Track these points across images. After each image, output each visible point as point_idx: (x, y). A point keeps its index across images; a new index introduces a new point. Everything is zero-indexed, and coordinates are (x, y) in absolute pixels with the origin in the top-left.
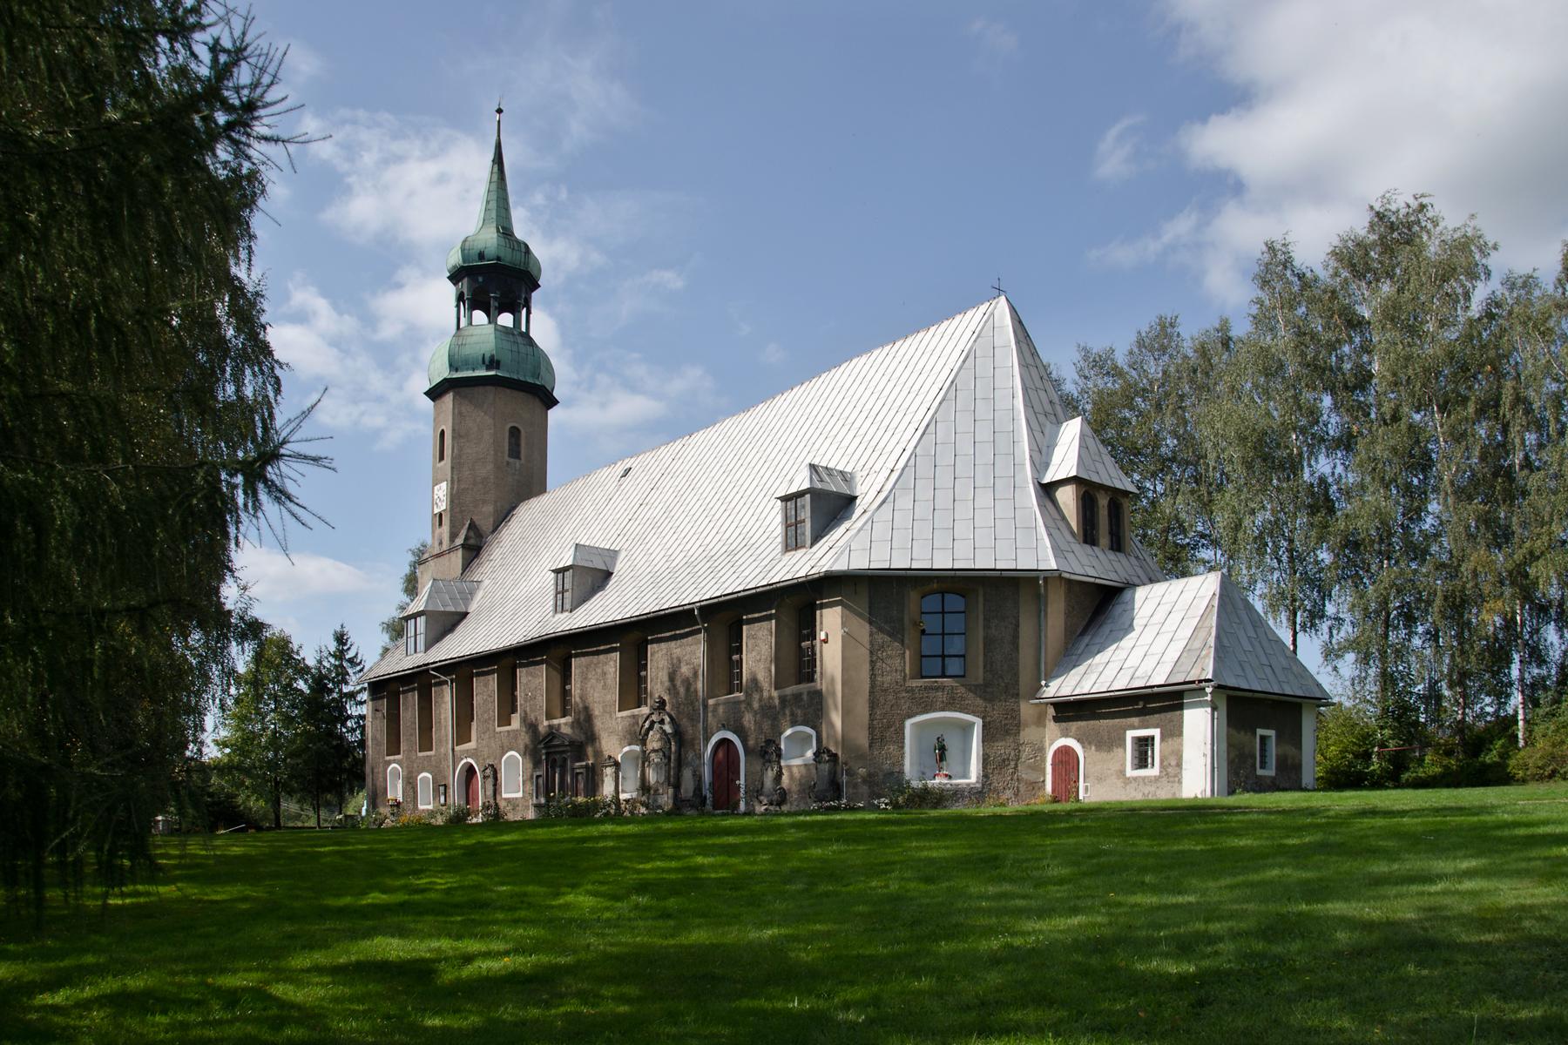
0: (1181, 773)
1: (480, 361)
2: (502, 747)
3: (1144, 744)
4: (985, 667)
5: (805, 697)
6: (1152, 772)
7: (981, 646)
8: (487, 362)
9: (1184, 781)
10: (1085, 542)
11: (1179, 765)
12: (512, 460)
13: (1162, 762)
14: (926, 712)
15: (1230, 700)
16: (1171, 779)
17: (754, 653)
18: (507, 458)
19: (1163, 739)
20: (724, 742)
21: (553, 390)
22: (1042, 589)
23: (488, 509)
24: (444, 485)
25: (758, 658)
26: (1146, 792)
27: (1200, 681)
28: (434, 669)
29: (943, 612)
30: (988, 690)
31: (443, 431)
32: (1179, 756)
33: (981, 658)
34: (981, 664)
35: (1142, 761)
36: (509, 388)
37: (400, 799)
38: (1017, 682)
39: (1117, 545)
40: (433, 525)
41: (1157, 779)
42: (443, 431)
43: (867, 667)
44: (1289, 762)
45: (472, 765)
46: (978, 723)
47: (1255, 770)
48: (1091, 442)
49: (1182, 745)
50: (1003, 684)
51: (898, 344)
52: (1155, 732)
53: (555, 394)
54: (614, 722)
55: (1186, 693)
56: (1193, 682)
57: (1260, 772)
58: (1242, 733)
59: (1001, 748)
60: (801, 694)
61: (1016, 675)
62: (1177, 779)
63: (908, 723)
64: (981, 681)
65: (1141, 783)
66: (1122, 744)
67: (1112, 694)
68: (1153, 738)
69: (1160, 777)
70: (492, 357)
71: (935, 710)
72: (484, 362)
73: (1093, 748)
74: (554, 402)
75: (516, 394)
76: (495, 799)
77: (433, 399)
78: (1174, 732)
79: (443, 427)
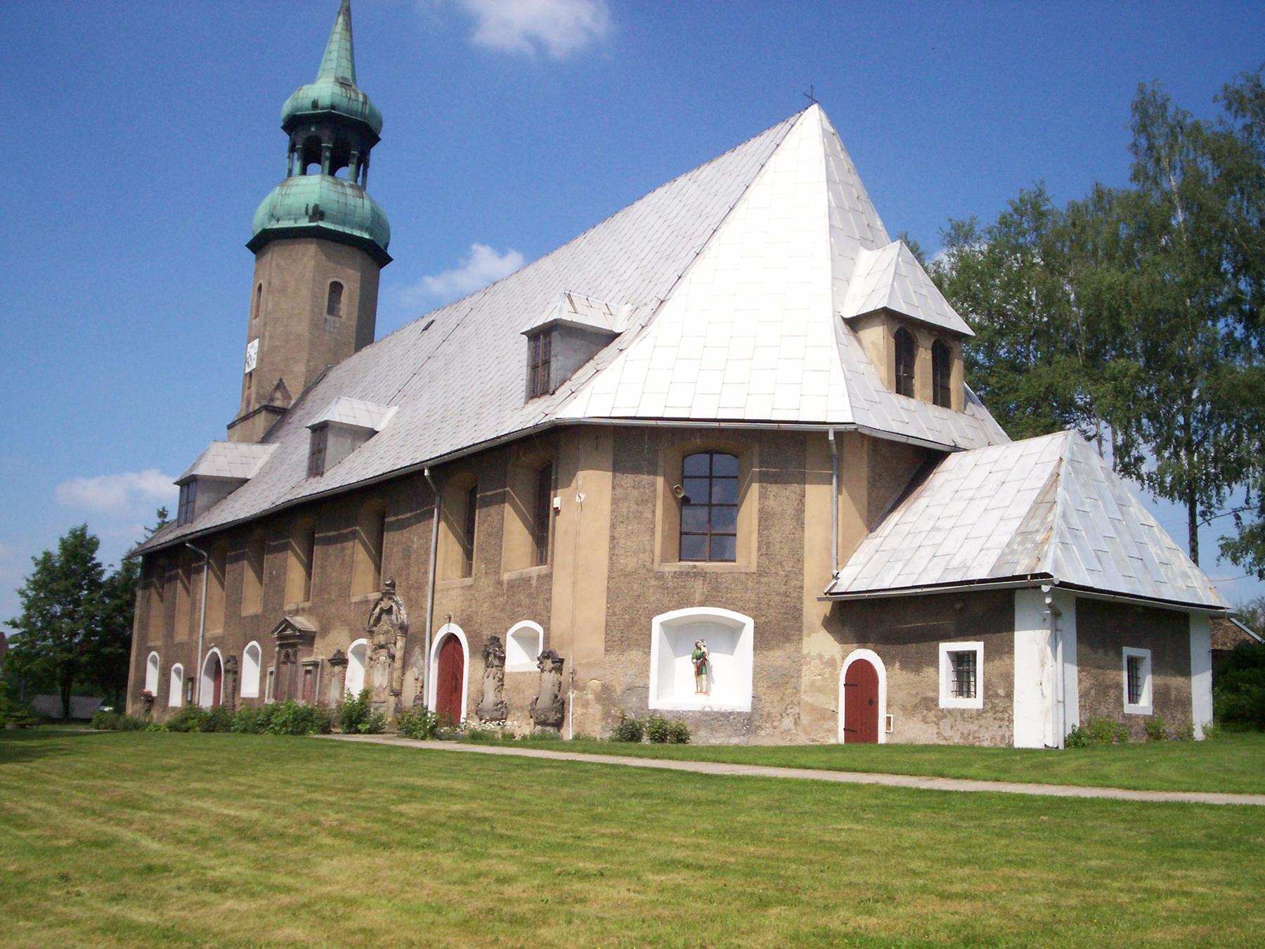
0: (1012, 705)
1: (304, 211)
2: (245, 635)
3: (963, 662)
4: (759, 549)
5: (534, 582)
6: (975, 702)
7: (755, 521)
8: (310, 211)
9: (1017, 717)
10: (898, 391)
11: (1009, 695)
12: (329, 317)
13: (986, 688)
14: (679, 606)
15: (532, 398)
16: (1000, 715)
17: (486, 525)
18: (325, 315)
19: (987, 658)
20: (451, 639)
21: (386, 247)
22: (834, 447)
23: (300, 369)
24: (256, 342)
25: (490, 530)
26: (966, 732)
27: (1034, 576)
28: (191, 541)
29: (711, 477)
30: (764, 580)
31: (260, 285)
32: (1008, 679)
33: (755, 537)
34: (755, 545)
35: (963, 686)
36: (332, 240)
37: (155, 694)
38: (801, 572)
39: (941, 397)
40: (244, 385)
41: (980, 714)
42: (260, 285)
43: (605, 543)
44: (1173, 694)
45: (216, 654)
46: (749, 623)
47: (1122, 706)
48: (904, 270)
49: (1012, 665)
50: (782, 573)
51: (702, 168)
52: (977, 646)
53: (390, 252)
54: (347, 608)
55: (1018, 594)
56: (1023, 577)
57: (1129, 708)
58: (1101, 651)
59: (777, 657)
60: (530, 579)
61: (800, 560)
62: (1006, 715)
63: (657, 621)
64: (754, 568)
65: (959, 718)
66: (934, 662)
67: (919, 590)
68: (974, 653)
69: (984, 711)
70: (316, 207)
71: (692, 605)
72: (307, 213)
73: (897, 665)
74: (388, 260)
75: (340, 247)
76: (233, 698)
77: (255, 251)
78: (1002, 650)
79: (261, 281)
